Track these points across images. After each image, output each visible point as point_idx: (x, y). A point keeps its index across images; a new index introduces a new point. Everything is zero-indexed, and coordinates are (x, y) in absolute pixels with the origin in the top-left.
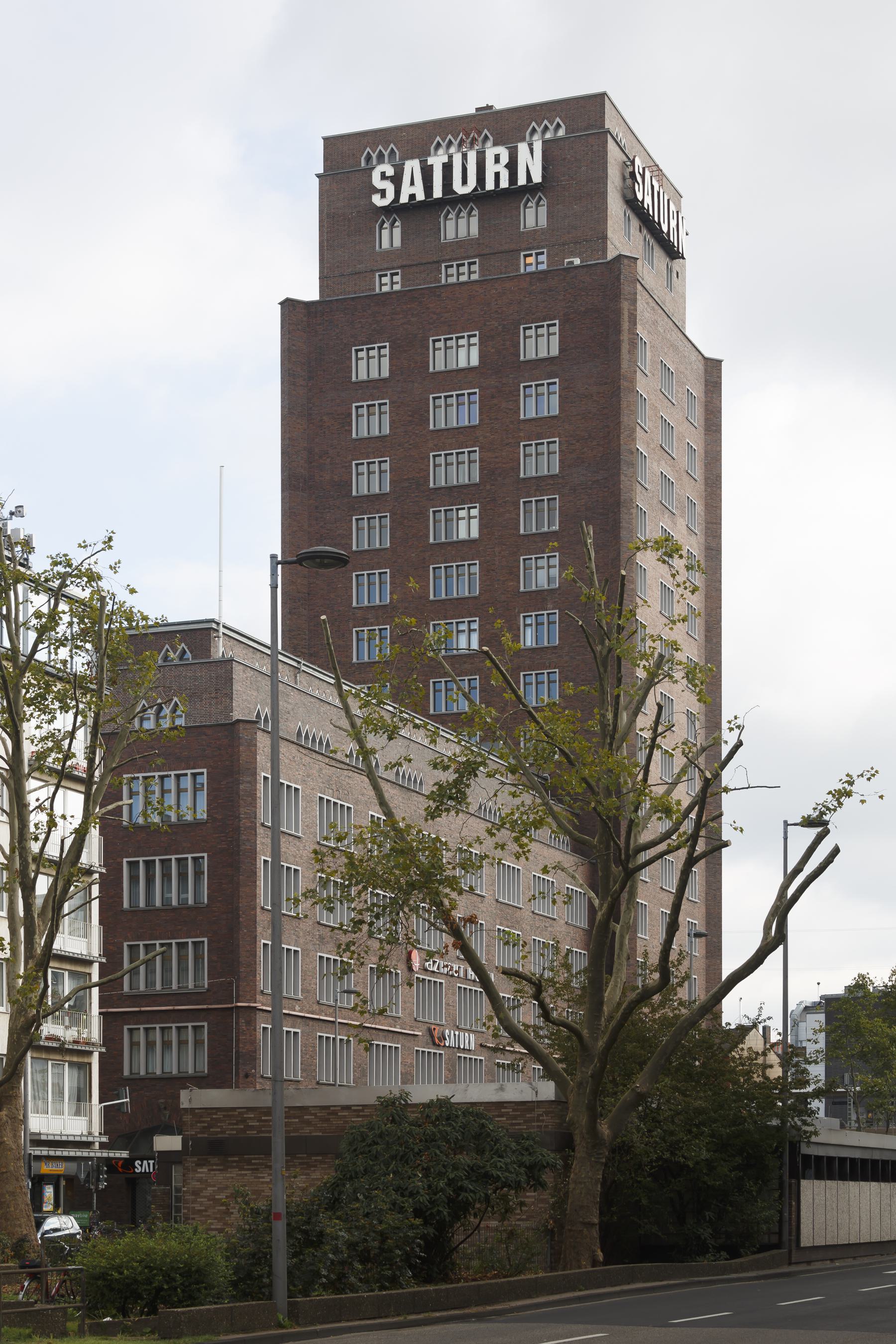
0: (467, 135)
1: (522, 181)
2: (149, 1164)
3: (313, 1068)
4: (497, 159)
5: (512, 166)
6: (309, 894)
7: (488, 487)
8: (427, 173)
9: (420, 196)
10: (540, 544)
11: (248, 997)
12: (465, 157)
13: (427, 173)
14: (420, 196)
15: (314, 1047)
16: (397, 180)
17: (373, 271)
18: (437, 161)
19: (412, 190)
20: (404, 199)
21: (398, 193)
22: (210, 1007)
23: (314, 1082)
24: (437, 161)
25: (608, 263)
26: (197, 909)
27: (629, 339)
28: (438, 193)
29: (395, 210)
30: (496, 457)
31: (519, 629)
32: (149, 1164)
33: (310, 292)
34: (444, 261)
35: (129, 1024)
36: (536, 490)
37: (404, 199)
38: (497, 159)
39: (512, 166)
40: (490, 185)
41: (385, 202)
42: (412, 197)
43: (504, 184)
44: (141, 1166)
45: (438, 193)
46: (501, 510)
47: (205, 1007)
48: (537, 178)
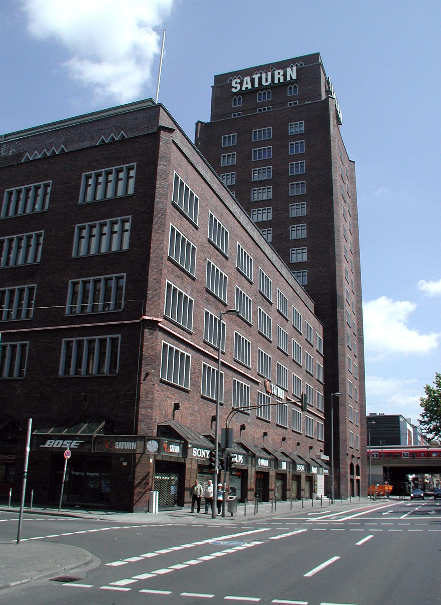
0: (272, 69)
1: (288, 79)
2: (122, 444)
3: (199, 384)
4: (279, 73)
5: (285, 75)
6: (202, 280)
7: (276, 180)
8: (253, 81)
9: (250, 87)
10: (298, 199)
11: (153, 313)
12: (267, 75)
13: (253, 81)
14: (250, 87)
15: (200, 371)
16: (241, 84)
17: (231, 113)
18: (256, 77)
19: (247, 86)
20: (244, 89)
21: (241, 87)
22: (124, 322)
23: (199, 396)
24: (256, 77)
25: (323, 101)
26: (120, 254)
27: (333, 124)
28: (256, 85)
29: (241, 93)
30: (279, 169)
31: (289, 232)
32: (122, 444)
33: (207, 119)
34: (258, 108)
35: (66, 338)
36: (296, 179)
37: (244, 89)
38: (279, 73)
39: (285, 75)
40: (276, 81)
41: (236, 91)
42: (247, 88)
43: (282, 81)
44: (118, 445)
45: (256, 85)
46: (282, 187)
47: (120, 322)
48: (294, 77)
